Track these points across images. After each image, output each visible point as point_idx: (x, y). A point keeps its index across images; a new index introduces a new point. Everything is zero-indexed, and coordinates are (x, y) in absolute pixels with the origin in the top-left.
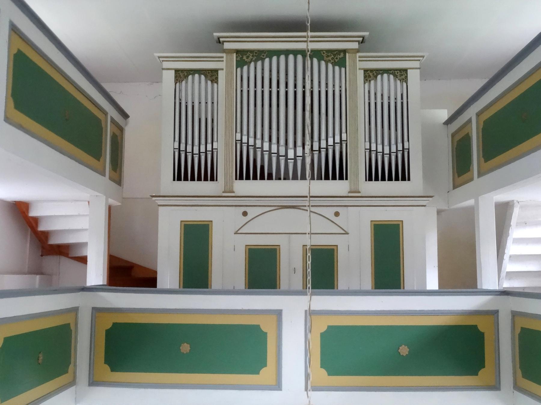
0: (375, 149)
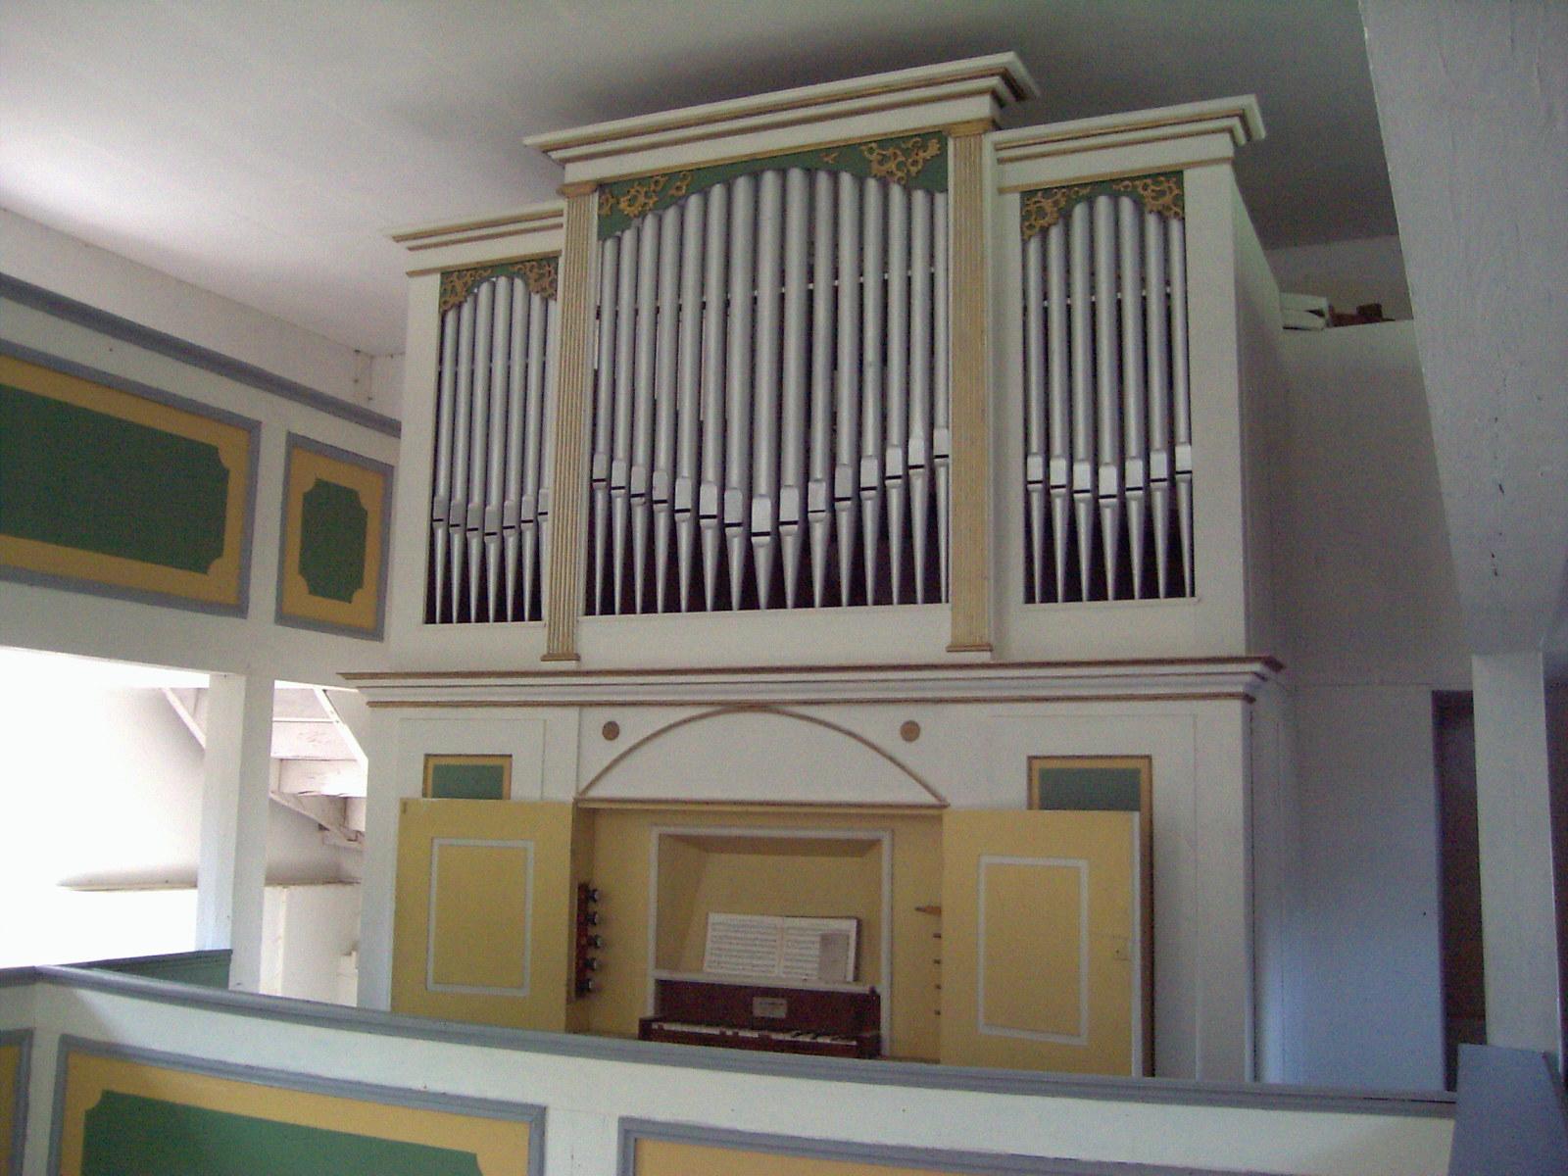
0: (1063, 481)
